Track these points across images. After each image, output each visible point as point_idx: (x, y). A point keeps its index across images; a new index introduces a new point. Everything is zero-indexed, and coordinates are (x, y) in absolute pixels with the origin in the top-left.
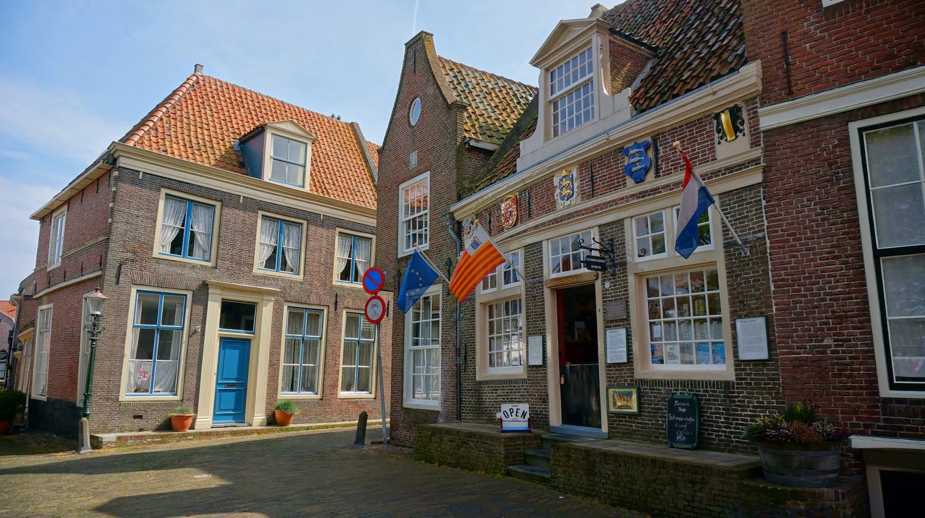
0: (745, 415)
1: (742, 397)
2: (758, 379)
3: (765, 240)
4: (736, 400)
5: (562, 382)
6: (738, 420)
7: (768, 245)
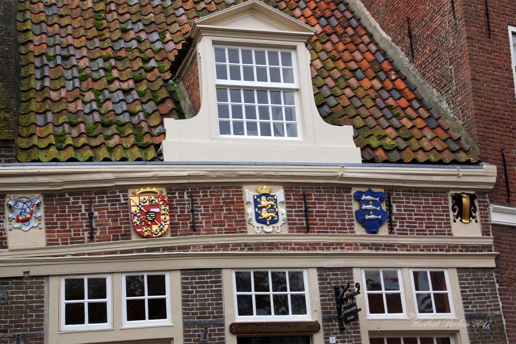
3: (501, 318)
7: (504, 323)
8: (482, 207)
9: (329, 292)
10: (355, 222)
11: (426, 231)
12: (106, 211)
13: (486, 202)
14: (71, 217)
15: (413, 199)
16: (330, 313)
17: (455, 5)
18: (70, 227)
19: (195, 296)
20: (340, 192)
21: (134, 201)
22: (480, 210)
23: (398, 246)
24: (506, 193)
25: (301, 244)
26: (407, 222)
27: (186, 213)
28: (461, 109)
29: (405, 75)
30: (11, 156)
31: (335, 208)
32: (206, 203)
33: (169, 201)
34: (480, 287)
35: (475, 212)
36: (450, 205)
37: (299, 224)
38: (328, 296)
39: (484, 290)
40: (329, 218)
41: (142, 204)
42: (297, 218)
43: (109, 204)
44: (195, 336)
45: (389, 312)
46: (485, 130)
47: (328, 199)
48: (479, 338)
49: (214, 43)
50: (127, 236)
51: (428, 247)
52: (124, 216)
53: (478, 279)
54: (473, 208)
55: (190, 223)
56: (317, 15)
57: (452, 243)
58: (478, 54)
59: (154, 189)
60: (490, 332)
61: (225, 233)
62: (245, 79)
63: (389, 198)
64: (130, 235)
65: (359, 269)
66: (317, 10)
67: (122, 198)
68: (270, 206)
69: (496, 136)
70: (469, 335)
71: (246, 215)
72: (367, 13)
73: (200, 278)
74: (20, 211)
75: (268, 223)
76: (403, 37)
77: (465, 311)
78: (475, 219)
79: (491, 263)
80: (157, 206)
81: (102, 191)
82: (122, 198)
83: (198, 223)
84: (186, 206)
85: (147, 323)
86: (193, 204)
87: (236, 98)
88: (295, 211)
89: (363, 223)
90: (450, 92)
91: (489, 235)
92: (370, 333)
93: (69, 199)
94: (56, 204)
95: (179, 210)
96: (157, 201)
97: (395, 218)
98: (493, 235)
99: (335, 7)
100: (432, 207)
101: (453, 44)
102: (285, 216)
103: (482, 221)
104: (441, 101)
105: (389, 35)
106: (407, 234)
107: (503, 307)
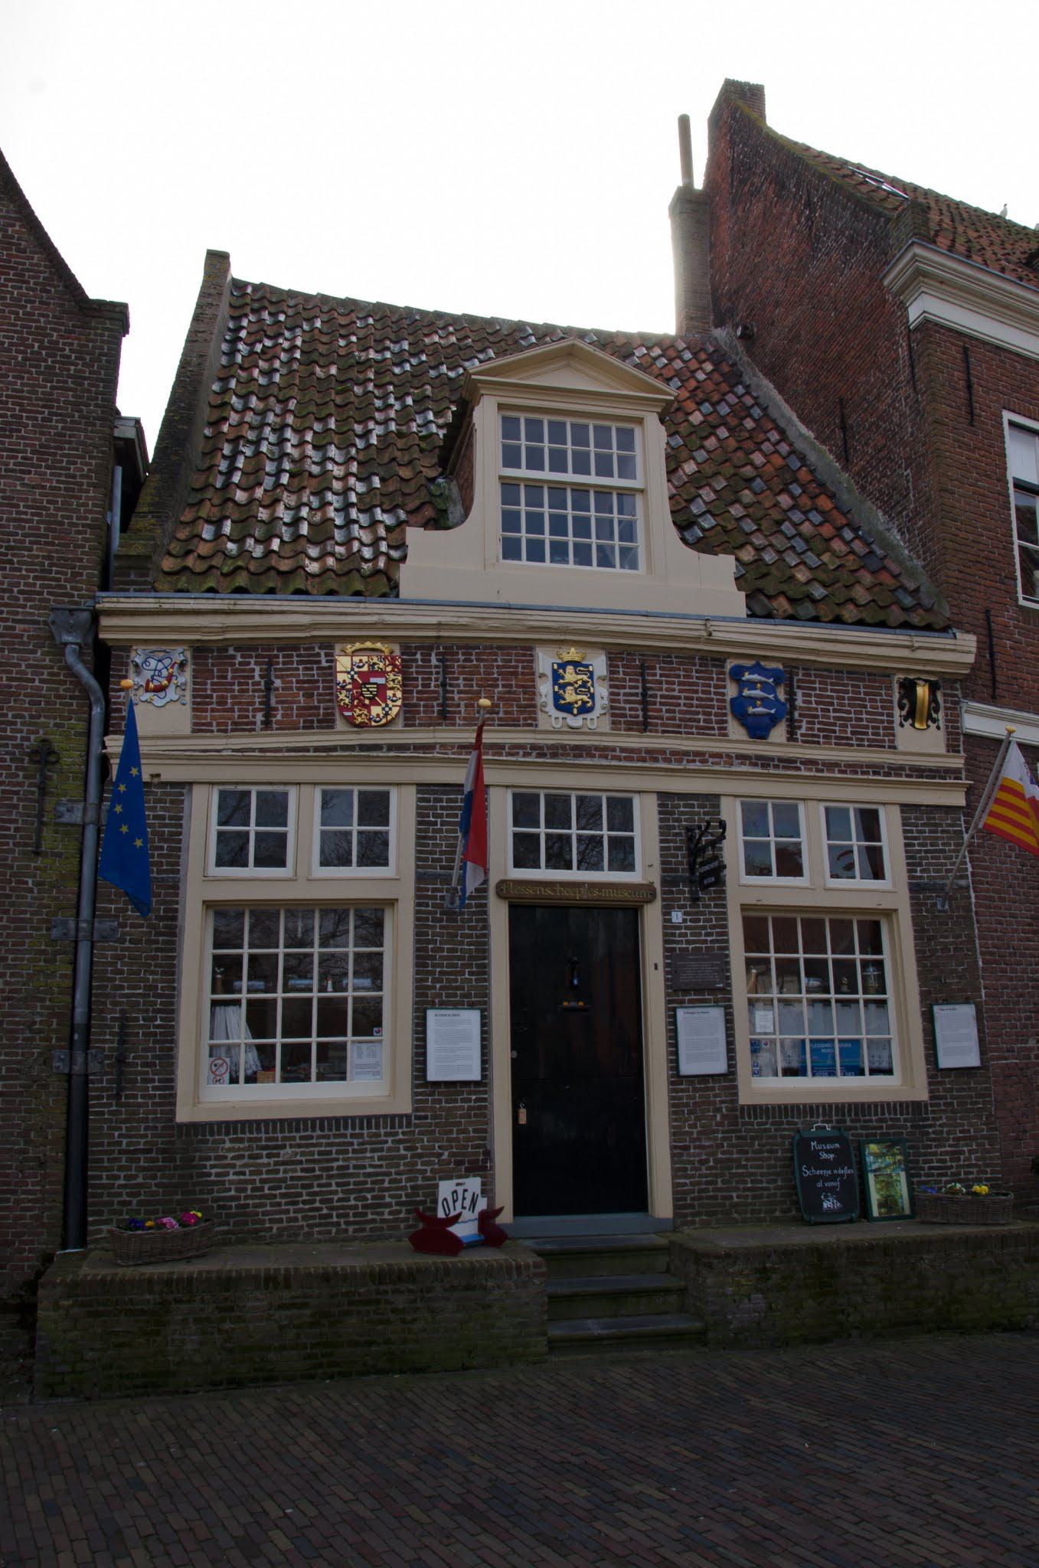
0: (942, 1154)
1: (940, 1125)
2: (963, 1097)
3: (969, 892)
4: (930, 1130)
5: (523, 1119)
6: (931, 1161)
7: (973, 900)
8: (949, 705)
9: (676, 835)
10: (729, 718)
11: (851, 739)
12: (294, 680)
13: (956, 696)
14: (236, 688)
15: (832, 684)
16: (677, 870)
17: (916, 370)
18: (233, 704)
19: (440, 831)
20: (706, 666)
21: (343, 663)
22: (946, 708)
23: (801, 763)
24: (989, 683)
25: (632, 750)
26: (819, 723)
27: (432, 688)
28: (921, 540)
29: (834, 490)
30: (145, 583)
31: (696, 692)
32: (470, 673)
33: (403, 666)
34: (937, 838)
35: (937, 711)
36: (896, 697)
37: (631, 716)
38: (675, 842)
39: (943, 844)
41: (356, 669)
42: (627, 706)
43: (301, 667)
44: (435, 898)
45: (779, 874)
46: (961, 575)
48: (929, 924)
49: (501, 407)
50: (327, 723)
51: (854, 767)
52: (324, 688)
53: (936, 825)
54: (933, 705)
55: (438, 705)
56: (697, 399)
58: (952, 450)
59: (379, 645)
61: (499, 725)
62: (551, 470)
63: (791, 680)
64: (333, 721)
65: (731, 798)
66: (698, 392)
67: (323, 659)
68: (580, 683)
69: (977, 587)
71: (537, 698)
72: (779, 398)
73: (449, 800)
74: (152, 673)
75: (575, 711)
76: (833, 430)
77: (910, 877)
79: (959, 799)
80: (382, 673)
81: (290, 646)
82: (323, 659)
83: (452, 706)
84: (433, 677)
85: (354, 871)
86: (445, 673)
87: (534, 500)
88: (625, 694)
89: (741, 716)
90: (904, 513)
91: (958, 752)
92: (744, 908)
93: (234, 657)
94: (213, 665)
95: (420, 682)
96: (381, 665)
97: (800, 715)
98: (965, 751)
99: (727, 389)
100: (864, 700)
101: (912, 434)
102: (606, 702)
103: (947, 727)
104: (889, 530)
105: (811, 429)
106: (818, 743)
107: (973, 874)
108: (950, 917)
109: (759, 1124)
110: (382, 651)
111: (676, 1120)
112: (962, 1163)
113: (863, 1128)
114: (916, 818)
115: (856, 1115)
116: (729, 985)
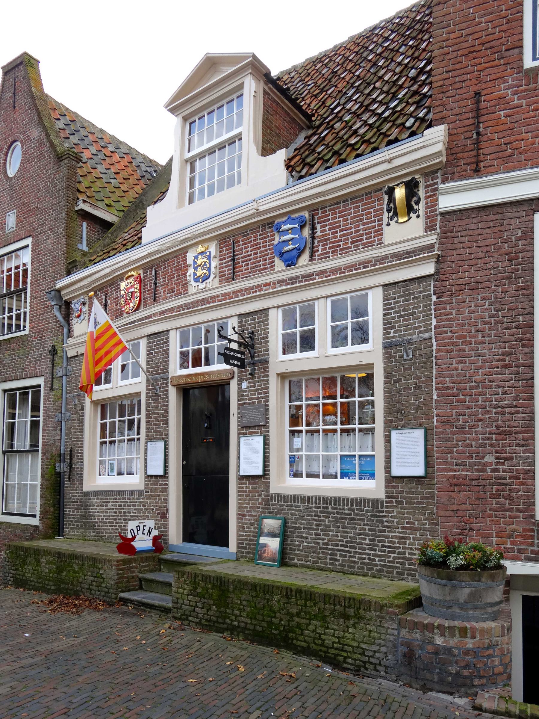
4: (385, 520)
7: (434, 347)
35: (417, 203)
40: (254, 260)
47: (254, 240)
51: (349, 268)
57: (380, 255)
59: (133, 273)
60: (413, 361)
68: (203, 263)
70: (385, 368)
78: (417, 214)
107: (436, 327)
108: (414, 364)
109: (280, 505)
110: (133, 275)
111: (240, 500)
112: (407, 546)
113: (338, 513)
114: (394, 293)
115: (335, 505)
116: (268, 423)
